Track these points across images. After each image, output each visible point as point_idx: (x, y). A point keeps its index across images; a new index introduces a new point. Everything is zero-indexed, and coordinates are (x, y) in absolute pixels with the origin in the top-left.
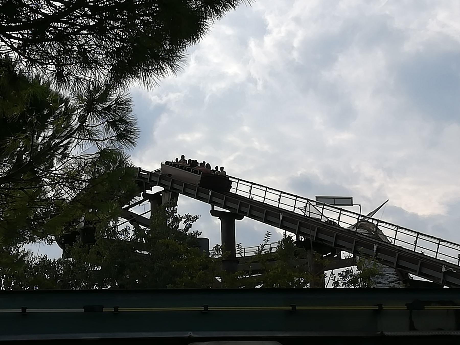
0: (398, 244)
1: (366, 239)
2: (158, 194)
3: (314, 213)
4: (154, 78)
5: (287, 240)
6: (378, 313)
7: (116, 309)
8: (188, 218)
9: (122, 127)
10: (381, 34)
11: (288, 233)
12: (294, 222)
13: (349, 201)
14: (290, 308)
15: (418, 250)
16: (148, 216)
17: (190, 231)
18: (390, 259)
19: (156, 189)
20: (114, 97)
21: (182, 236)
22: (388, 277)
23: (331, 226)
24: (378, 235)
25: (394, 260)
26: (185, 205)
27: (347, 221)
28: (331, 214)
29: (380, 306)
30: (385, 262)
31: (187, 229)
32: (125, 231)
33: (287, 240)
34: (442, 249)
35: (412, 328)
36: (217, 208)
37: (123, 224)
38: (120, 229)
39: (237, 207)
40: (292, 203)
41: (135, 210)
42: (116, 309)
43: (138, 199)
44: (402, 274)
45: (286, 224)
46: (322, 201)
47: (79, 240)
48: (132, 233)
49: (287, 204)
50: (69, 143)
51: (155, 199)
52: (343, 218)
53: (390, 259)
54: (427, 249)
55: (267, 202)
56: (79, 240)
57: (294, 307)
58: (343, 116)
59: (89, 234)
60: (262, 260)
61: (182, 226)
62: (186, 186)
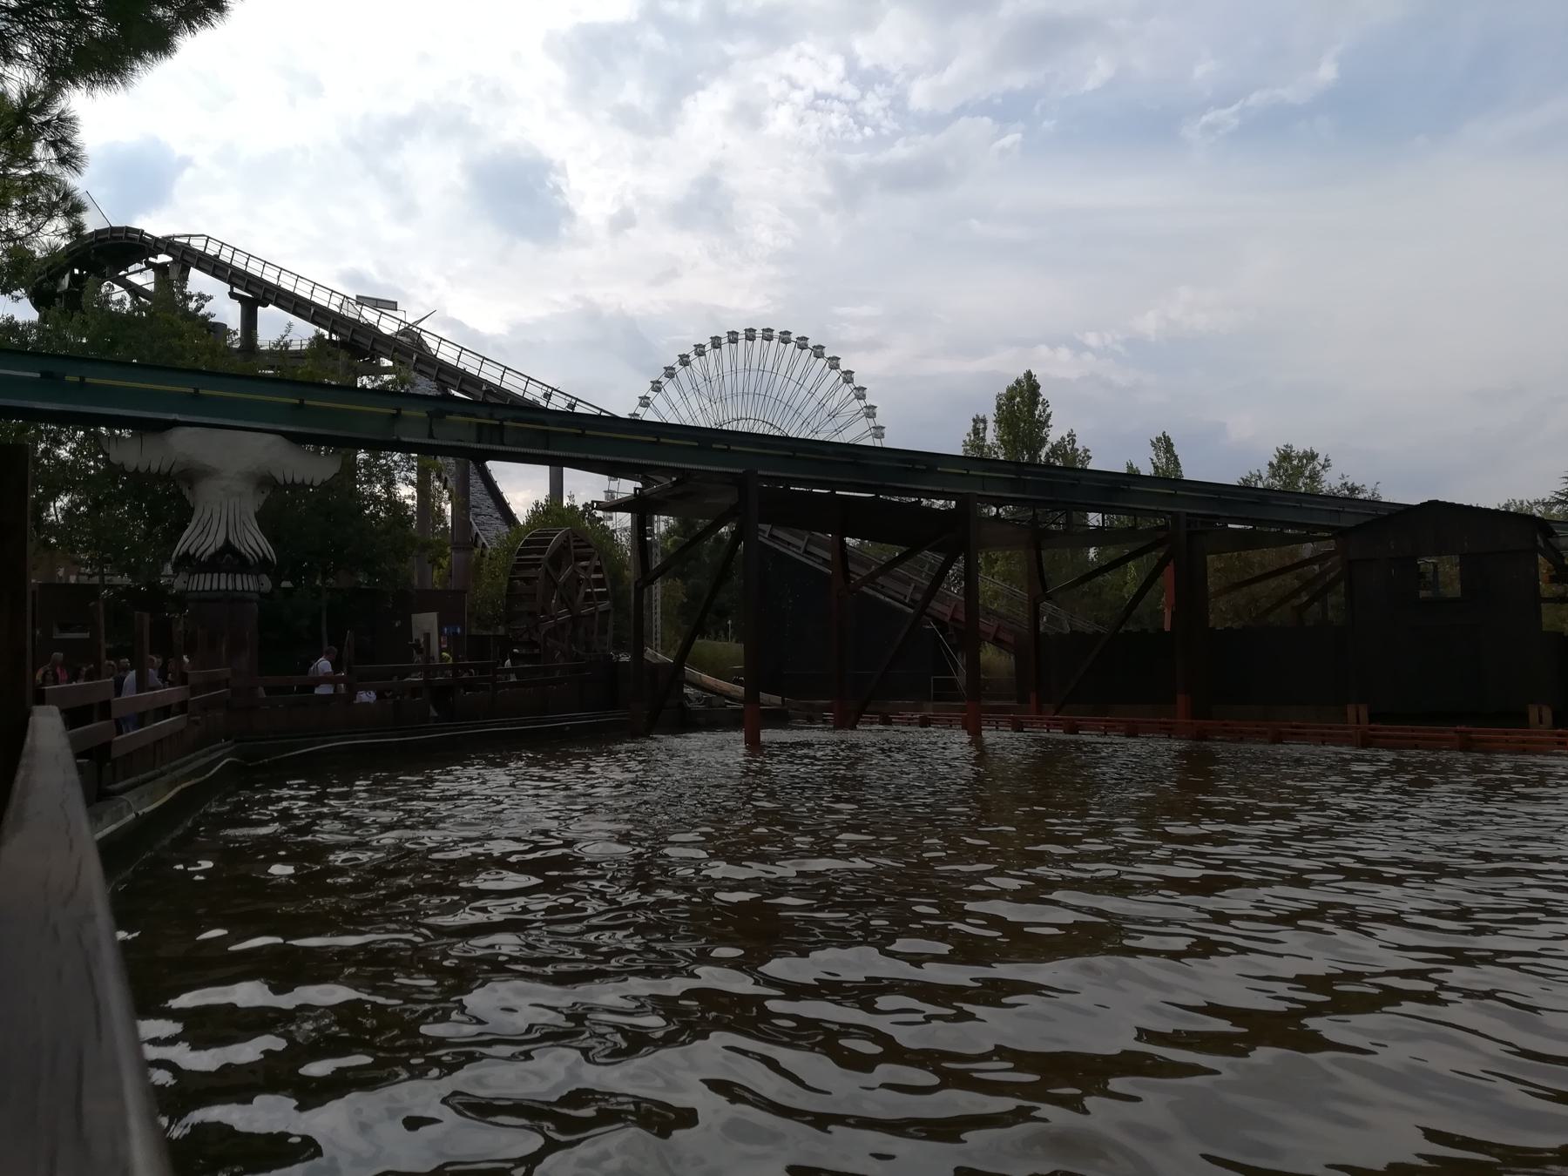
0: (440, 356)
1: (409, 348)
2: (164, 265)
3: (351, 312)
4: (100, 92)
5: (319, 337)
6: (396, 417)
7: (82, 379)
8: (201, 296)
9: (66, 149)
10: (452, 126)
11: (322, 330)
12: (327, 319)
13: (393, 306)
15: (461, 366)
16: (151, 287)
17: (202, 312)
19: (163, 258)
20: (56, 112)
21: (192, 316)
22: (426, 386)
23: (371, 330)
24: (420, 344)
25: (434, 373)
26: (198, 281)
27: (388, 327)
28: (370, 316)
29: (399, 410)
30: (421, 372)
31: (198, 309)
32: (121, 302)
33: (319, 337)
35: (431, 436)
36: (236, 290)
37: (118, 293)
38: (115, 297)
39: (261, 292)
41: (137, 279)
42: (82, 379)
43: (137, 266)
44: (444, 386)
46: (361, 301)
47: (60, 304)
48: (128, 306)
49: (321, 298)
51: (160, 269)
54: (470, 365)
56: (60, 304)
58: (406, 212)
59: (74, 299)
60: (282, 353)
61: (192, 305)
62: (278, 296)
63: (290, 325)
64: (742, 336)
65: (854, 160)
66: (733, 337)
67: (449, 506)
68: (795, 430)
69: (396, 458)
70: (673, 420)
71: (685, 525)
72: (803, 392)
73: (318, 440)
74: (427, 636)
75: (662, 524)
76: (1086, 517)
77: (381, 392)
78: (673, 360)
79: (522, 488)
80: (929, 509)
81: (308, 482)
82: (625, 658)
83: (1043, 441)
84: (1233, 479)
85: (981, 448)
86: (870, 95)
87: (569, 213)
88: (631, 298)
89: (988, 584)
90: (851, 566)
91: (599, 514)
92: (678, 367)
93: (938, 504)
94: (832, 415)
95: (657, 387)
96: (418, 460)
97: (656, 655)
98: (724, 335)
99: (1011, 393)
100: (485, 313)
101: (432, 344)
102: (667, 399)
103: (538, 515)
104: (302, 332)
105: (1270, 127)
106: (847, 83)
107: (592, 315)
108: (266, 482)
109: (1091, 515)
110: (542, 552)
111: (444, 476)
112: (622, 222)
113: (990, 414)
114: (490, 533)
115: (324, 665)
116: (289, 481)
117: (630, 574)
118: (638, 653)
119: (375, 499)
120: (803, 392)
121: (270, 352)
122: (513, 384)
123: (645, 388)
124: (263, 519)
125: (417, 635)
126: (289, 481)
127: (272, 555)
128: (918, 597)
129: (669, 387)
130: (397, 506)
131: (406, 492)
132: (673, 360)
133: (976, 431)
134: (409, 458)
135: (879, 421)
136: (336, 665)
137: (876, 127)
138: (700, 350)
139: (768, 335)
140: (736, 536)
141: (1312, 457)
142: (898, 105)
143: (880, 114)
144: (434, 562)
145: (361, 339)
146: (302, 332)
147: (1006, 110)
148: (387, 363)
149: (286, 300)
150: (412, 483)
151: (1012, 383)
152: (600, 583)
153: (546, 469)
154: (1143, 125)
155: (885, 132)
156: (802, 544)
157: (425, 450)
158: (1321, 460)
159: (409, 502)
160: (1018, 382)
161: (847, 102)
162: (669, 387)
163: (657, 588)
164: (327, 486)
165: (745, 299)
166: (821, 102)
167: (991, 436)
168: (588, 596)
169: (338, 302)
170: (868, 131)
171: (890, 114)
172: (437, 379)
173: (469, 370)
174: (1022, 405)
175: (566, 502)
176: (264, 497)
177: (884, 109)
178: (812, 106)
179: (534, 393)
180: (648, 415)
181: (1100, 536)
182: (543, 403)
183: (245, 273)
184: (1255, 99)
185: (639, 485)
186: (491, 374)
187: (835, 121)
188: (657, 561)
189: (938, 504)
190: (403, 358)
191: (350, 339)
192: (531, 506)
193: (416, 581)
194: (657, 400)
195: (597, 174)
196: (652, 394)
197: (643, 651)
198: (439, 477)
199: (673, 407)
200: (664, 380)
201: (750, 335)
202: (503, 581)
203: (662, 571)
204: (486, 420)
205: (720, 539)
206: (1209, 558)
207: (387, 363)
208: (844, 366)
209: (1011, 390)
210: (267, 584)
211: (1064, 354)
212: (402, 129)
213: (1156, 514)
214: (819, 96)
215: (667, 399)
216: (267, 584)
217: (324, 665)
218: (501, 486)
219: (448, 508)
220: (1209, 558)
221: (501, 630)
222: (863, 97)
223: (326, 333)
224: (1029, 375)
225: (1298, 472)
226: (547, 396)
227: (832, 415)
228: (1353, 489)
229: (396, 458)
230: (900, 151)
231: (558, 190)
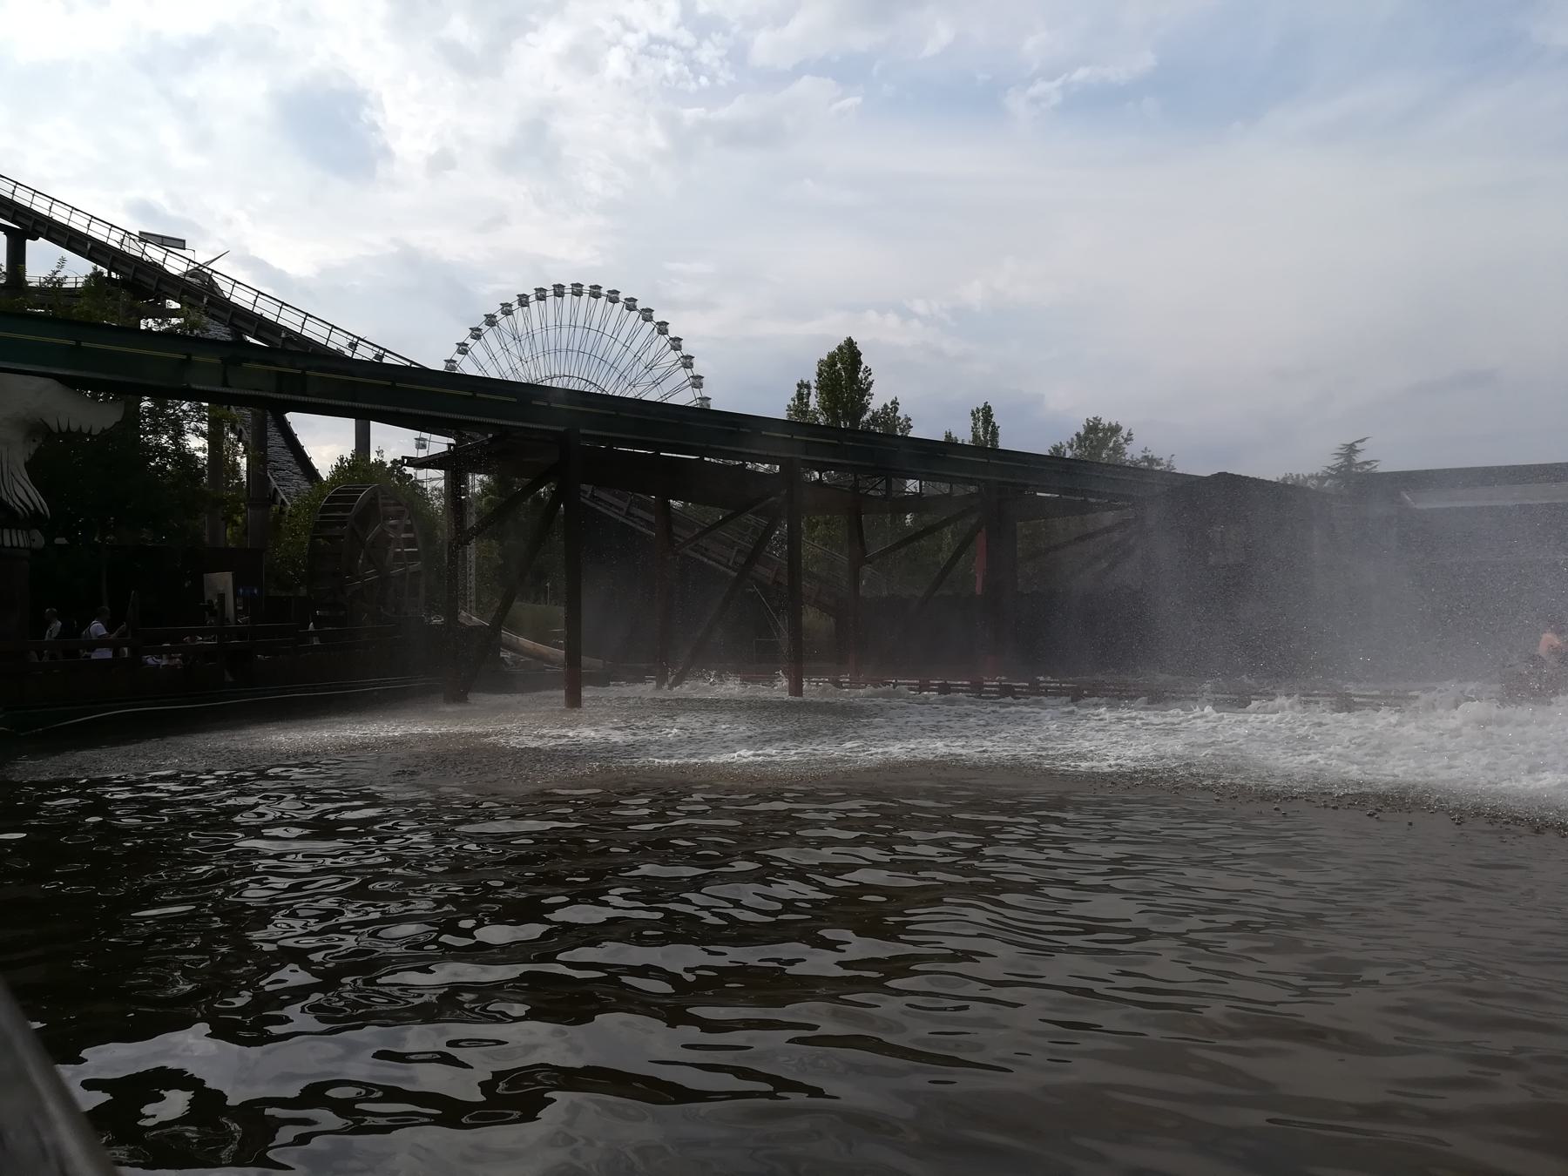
0: (233, 299)
1: (199, 289)
3: (134, 249)
5: (96, 275)
6: (187, 363)
11: (99, 268)
12: (64, 235)
13: (181, 244)
14: (73, 343)
15: (257, 311)
18: (223, 315)
22: (219, 332)
23: (156, 269)
25: (227, 317)
27: (175, 266)
28: (154, 253)
29: (189, 356)
30: (213, 317)
34: (36, 200)
35: (225, 384)
39: (30, 224)
40: (67, 214)
44: (238, 333)
45: (96, 256)
46: (145, 238)
49: (99, 232)
50: (962, 808)
52: (237, 292)
53: (223, 315)
54: (268, 311)
55: (34, 207)
57: (79, 342)
60: (53, 291)
63: (63, 260)
64: (568, 290)
65: (691, 114)
66: (559, 291)
67: (245, 460)
68: (613, 387)
69: (185, 407)
70: (494, 375)
71: (501, 484)
72: (618, 346)
73: (96, 386)
74: (222, 597)
75: (477, 482)
76: (904, 484)
77: (169, 334)
78: (495, 309)
79: (325, 441)
80: (754, 473)
81: (85, 430)
82: (437, 621)
83: (864, 408)
84: (1044, 450)
85: (805, 413)
86: (706, 44)
87: (387, 153)
88: (451, 245)
89: (810, 549)
90: (675, 529)
91: (409, 470)
92: (499, 316)
93: (763, 467)
94: (649, 367)
95: (476, 334)
96: (209, 410)
97: (470, 618)
98: (531, 292)
99: (832, 360)
100: (284, 254)
101: (225, 287)
102: (487, 348)
103: (341, 470)
104: (77, 270)
105: (1095, 105)
106: (682, 29)
107: (410, 259)
108: (38, 430)
109: (909, 482)
110: (349, 509)
111: (238, 427)
112: (441, 163)
113: (812, 378)
114: (289, 490)
115: (97, 628)
116: (64, 429)
117: (444, 533)
118: (452, 614)
119: (162, 451)
120: (618, 346)
121: (40, 290)
122: (315, 332)
123: (464, 335)
124: (33, 467)
125: (209, 595)
126: (64, 429)
127: (45, 509)
128: (742, 560)
129: (489, 334)
130: (188, 458)
131: (196, 444)
132: (495, 309)
133: (800, 396)
134: (200, 408)
135: (696, 371)
136: (110, 628)
137: (713, 78)
138: (523, 300)
139: (595, 292)
140: (556, 497)
141: (1115, 430)
142: (737, 55)
143: (716, 64)
144: (228, 519)
145: (146, 279)
146: (77, 270)
147: (846, 71)
148: (175, 305)
149: (59, 233)
150: (203, 434)
151: (833, 348)
152: (410, 543)
153: (352, 421)
154: (969, 96)
155: (721, 82)
156: (624, 506)
157: (216, 399)
158: (1124, 433)
159: (200, 454)
160: (840, 348)
161: (682, 49)
162: (489, 334)
163: (472, 551)
164: (106, 435)
165: (573, 253)
166: (655, 48)
167: (813, 402)
168: (398, 556)
169: (119, 238)
170: (703, 80)
171: (727, 64)
172: (231, 324)
173: (266, 315)
174: (844, 371)
175: (373, 457)
176: (35, 446)
177: (721, 59)
178: (645, 51)
179: (338, 342)
180: (467, 367)
181: (917, 503)
182: (348, 353)
183: (12, 202)
184: (1081, 74)
185: (452, 441)
186: (291, 321)
187: (670, 68)
188: (472, 521)
189: (763, 467)
190: (193, 302)
191: (130, 279)
192: (335, 462)
193: (207, 539)
194: (476, 347)
195: (416, 113)
196: (470, 342)
197: (456, 614)
198: (233, 429)
199: (493, 357)
200: (484, 328)
201: (577, 290)
202: (305, 538)
203: (478, 532)
204: (286, 369)
205: (538, 500)
206: (1019, 524)
207: (175, 305)
208: (657, 317)
209: (832, 356)
210: (39, 540)
211: (892, 320)
212: (201, 50)
213: (971, 482)
214: (653, 40)
215: (487, 348)
216: (39, 540)
217: (97, 628)
218: (302, 440)
219: (243, 462)
220: (1019, 524)
221: (303, 591)
222: (699, 45)
223: (105, 271)
224: (850, 343)
225: (1103, 443)
226: (353, 346)
227: (649, 367)
228: (1151, 460)
229: (185, 407)
230: (735, 110)
231: (374, 127)
